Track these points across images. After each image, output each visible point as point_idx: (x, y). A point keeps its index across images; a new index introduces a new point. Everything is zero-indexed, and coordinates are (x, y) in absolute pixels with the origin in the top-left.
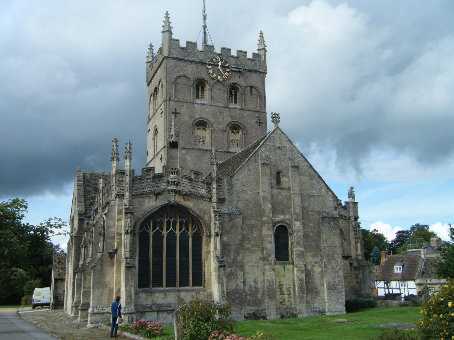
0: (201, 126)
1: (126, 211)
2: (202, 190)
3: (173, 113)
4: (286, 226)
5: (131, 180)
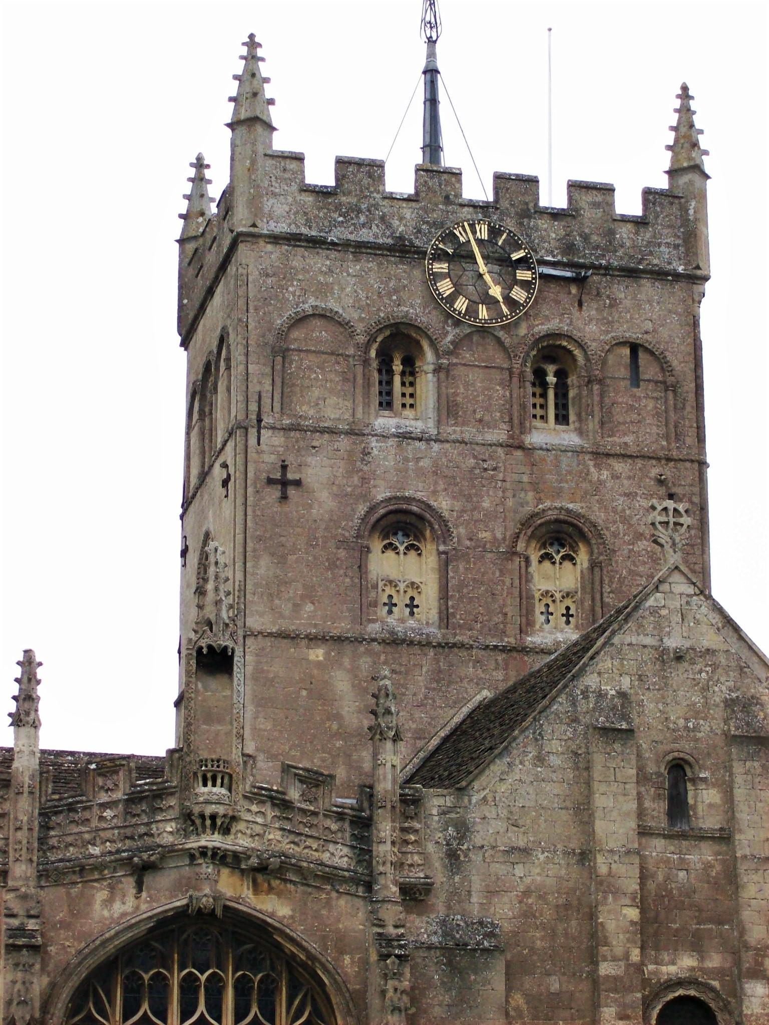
0: (400, 533)
1: (11, 941)
2: (331, 847)
3: (270, 481)
4: (707, 1000)
5: (37, 811)
